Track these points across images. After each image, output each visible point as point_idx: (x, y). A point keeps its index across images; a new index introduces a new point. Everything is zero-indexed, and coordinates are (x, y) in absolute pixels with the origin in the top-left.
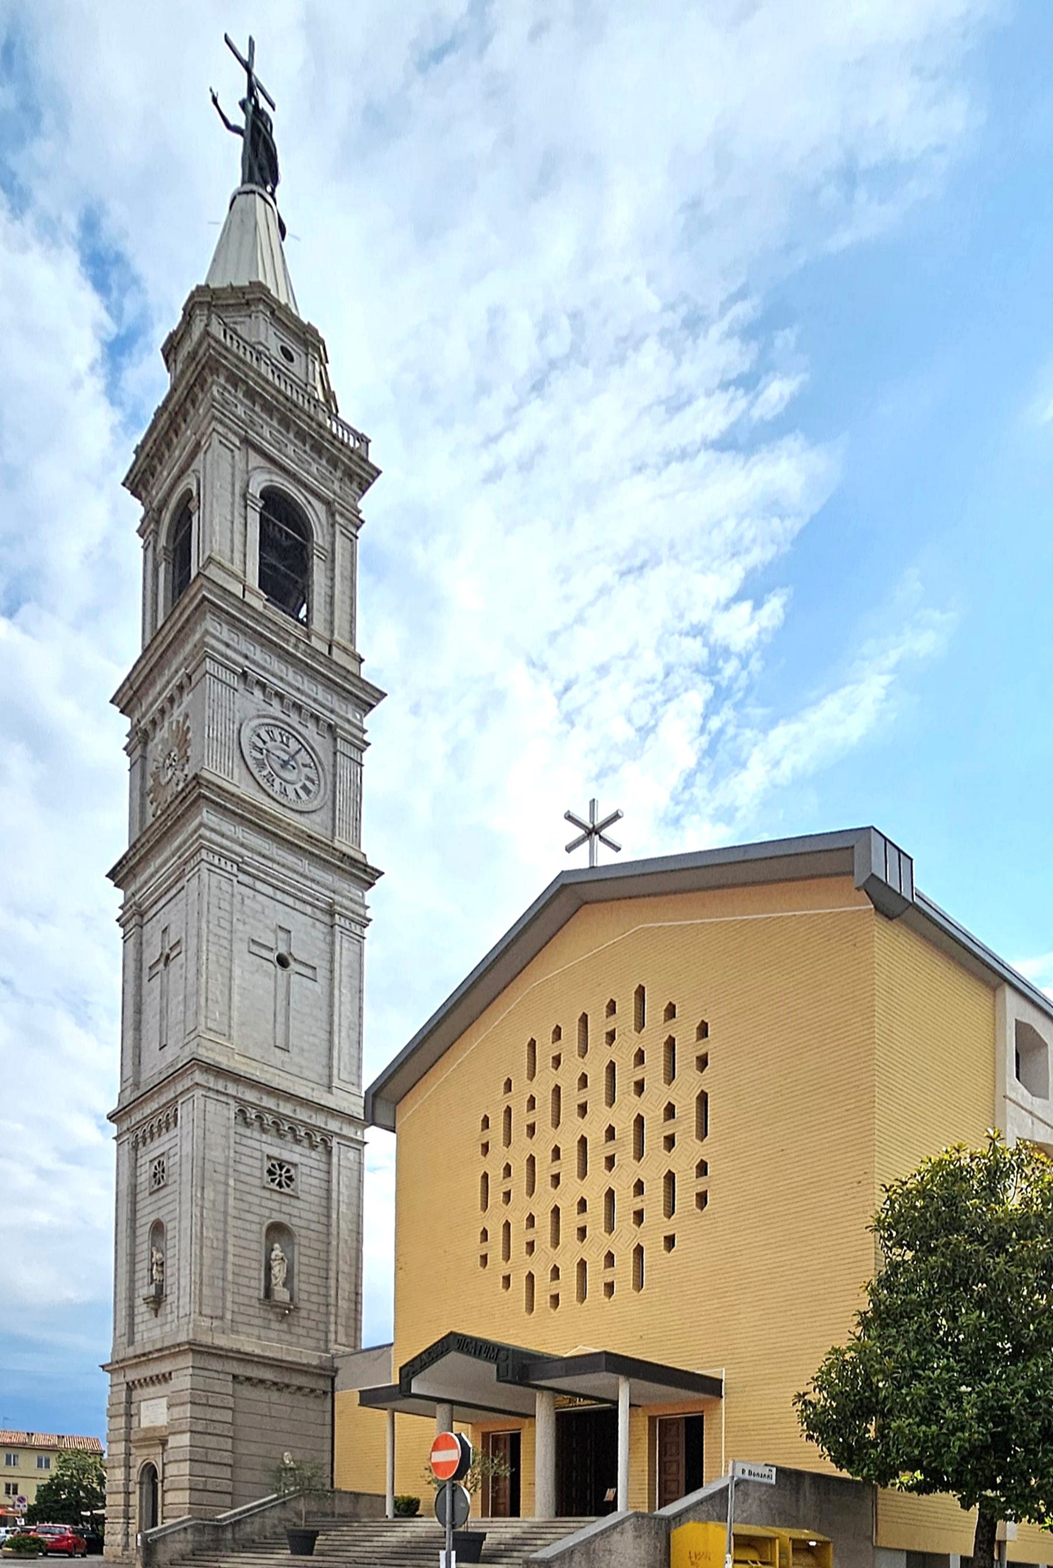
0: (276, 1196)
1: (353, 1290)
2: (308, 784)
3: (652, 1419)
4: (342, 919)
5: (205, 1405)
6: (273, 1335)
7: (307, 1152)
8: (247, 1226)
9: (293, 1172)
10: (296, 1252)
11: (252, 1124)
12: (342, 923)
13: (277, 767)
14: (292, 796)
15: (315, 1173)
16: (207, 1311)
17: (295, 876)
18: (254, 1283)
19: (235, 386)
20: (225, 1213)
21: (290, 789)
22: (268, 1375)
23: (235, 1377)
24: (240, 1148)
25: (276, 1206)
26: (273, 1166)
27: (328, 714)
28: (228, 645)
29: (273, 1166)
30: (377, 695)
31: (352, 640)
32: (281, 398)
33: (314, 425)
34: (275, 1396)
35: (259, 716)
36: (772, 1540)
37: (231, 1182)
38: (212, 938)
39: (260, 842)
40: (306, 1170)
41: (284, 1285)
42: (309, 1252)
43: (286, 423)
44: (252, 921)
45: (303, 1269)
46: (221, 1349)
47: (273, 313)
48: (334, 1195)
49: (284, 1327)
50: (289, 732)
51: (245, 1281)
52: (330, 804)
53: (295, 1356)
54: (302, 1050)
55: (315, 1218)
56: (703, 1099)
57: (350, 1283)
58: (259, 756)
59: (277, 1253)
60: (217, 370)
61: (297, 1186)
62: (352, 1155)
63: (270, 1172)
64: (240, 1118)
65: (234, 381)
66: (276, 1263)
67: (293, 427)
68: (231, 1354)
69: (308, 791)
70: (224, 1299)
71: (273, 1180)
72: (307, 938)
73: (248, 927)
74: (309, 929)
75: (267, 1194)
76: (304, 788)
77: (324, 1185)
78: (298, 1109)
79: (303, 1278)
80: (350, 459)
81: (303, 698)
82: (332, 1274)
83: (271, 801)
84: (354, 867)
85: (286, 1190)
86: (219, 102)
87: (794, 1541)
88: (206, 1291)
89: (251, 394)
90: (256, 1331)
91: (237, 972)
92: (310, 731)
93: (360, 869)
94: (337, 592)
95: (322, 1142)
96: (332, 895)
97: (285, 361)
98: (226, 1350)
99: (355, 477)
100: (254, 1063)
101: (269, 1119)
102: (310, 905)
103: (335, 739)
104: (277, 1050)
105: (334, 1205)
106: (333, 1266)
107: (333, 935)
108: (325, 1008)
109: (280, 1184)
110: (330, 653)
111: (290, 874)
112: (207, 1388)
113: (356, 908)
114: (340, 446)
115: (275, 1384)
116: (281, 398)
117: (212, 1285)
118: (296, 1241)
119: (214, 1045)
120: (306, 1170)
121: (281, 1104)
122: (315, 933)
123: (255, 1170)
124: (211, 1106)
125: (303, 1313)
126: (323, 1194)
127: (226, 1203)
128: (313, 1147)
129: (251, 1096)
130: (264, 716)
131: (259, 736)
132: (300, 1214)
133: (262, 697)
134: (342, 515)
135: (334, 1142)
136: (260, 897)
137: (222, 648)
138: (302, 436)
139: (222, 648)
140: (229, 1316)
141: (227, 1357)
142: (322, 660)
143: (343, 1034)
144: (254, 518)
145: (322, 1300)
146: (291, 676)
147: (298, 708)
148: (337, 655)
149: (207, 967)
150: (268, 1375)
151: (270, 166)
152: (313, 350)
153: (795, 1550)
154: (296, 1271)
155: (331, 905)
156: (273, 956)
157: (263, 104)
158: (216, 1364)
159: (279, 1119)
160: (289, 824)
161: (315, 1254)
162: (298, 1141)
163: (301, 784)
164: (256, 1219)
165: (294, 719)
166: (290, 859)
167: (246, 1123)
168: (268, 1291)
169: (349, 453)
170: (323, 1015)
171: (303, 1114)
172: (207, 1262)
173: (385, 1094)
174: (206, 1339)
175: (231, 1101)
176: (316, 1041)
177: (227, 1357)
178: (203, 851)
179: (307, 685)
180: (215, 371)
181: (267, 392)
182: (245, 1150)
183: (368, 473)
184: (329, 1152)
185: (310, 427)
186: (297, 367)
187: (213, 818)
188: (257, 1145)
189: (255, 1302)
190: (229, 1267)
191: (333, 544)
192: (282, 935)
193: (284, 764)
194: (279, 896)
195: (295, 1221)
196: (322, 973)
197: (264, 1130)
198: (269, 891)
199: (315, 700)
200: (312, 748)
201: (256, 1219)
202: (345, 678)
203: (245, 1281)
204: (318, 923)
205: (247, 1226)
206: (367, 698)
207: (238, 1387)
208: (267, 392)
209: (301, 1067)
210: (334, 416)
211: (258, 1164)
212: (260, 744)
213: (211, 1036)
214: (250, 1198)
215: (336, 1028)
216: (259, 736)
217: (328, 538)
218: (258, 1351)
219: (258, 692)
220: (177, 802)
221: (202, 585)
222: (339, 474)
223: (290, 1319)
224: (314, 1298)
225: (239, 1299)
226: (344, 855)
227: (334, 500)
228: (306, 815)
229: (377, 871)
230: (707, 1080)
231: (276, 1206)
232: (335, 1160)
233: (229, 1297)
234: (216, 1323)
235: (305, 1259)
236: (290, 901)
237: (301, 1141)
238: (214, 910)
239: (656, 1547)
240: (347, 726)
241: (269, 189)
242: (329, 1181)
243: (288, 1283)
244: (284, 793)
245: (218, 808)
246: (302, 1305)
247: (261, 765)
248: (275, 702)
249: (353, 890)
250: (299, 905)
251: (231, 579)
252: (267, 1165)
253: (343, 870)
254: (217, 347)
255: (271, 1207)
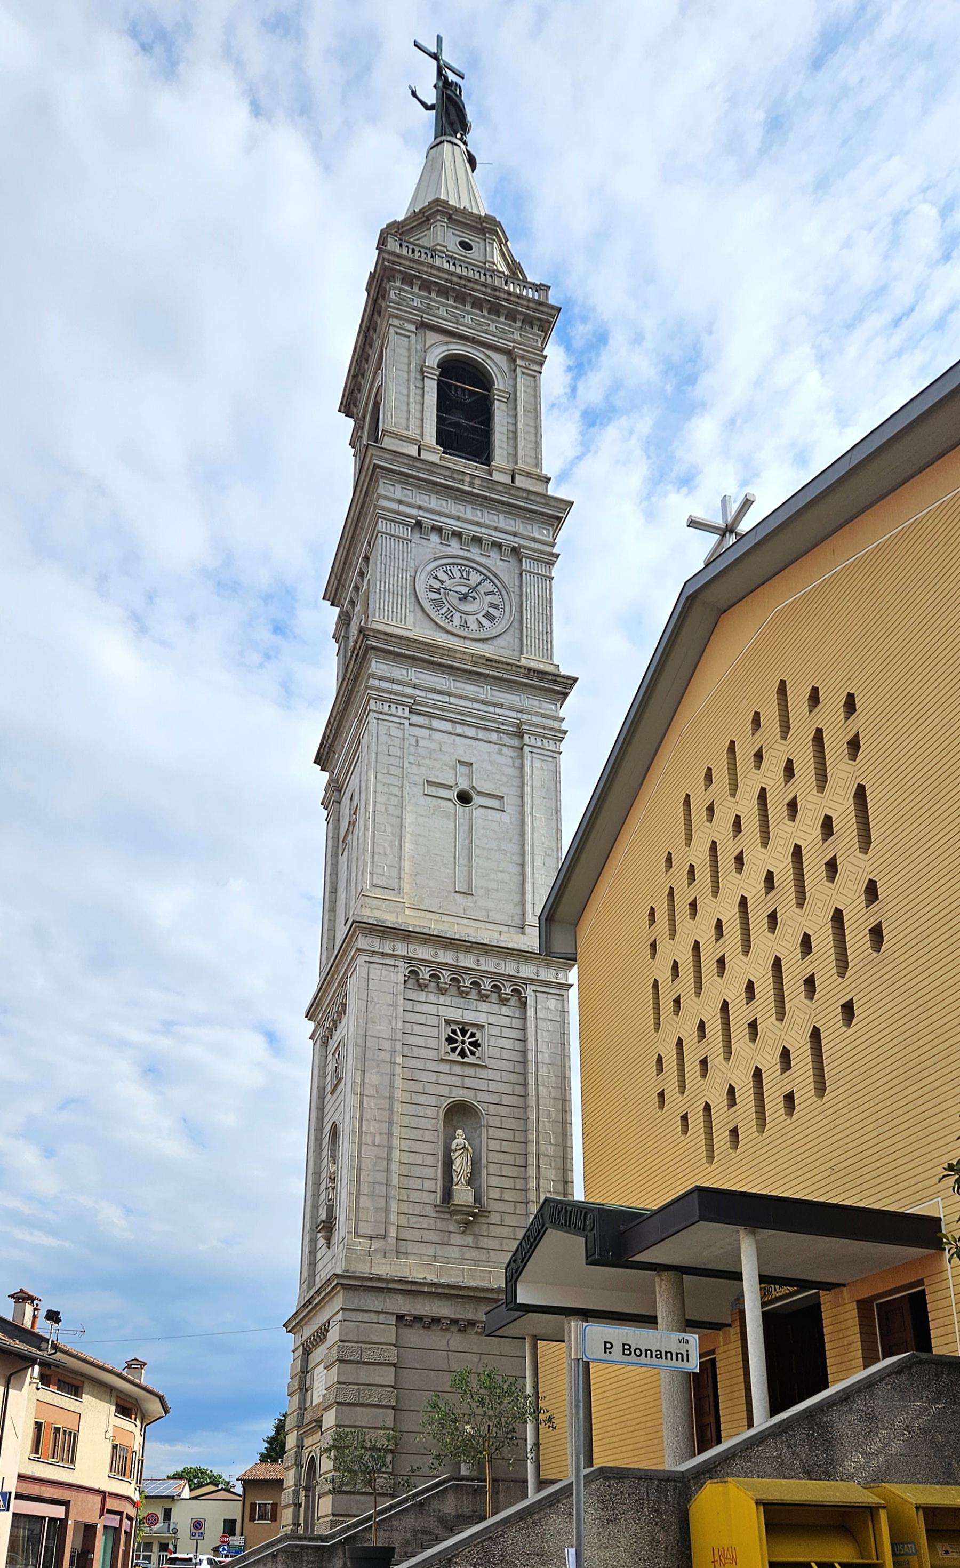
0: (457, 1069)
1: (560, 1177)
2: (492, 611)
3: (864, 1306)
4: (532, 738)
5: (357, 1362)
6: (454, 1252)
7: (495, 1008)
8: (421, 1111)
9: (478, 1036)
10: (484, 1136)
11: (426, 986)
12: (533, 742)
13: (455, 602)
14: (474, 626)
15: (507, 1033)
16: (366, 1229)
17: (476, 705)
18: (428, 1185)
19: (411, 285)
20: (391, 1098)
21: (471, 620)
22: (444, 1310)
23: (400, 1318)
24: (411, 1017)
25: (457, 1081)
26: (454, 1032)
27: (511, 538)
28: (420, 508)
29: (454, 1032)
30: (563, 506)
31: (538, 463)
32: (455, 279)
33: (489, 291)
34: (456, 1340)
35: (435, 559)
36: (871, 1511)
37: (399, 1060)
38: (380, 788)
39: (437, 679)
40: (495, 1031)
41: (469, 1182)
42: (501, 1134)
43: (461, 298)
44: (427, 761)
45: (495, 1157)
46: (380, 1279)
47: (450, 218)
48: (531, 1056)
49: (469, 1240)
50: (467, 565)
51: (417, 1184)
52: (516, 625)
53: (482, 1279)
54: (488, 890)
55: (507, 1089)
56: (860, 794)
57: (557, 1169)
58: (437, 596)
59: (460, 1141)
60: (394, 277)
61: (483, 1052)
62: (552, 1003)
63: (450, 1040)
64: (411, 982)
65: (408, 280)
66: (457, 1154)
67: (469, 299)
68: (391, 1286)
69: (496, 607)
70: (387, 1211)
71: (453, 1050)
72: (490, 763)
73: (422, 769)
74: (495, 757)
75: (444, 1067)
76: (492, 605)
77: (518, 1046)
78: (482, 960)
79: (493, 1169)
80: (528, 308)
81: (483, 530)
82: (532, 1160)
83: (450, 637)
84: (542, 680)
85: (470, 1059)
86: (417, 93)
87: (931, 1513)
88: (365, 1202)
89: (426, 286)
90: (430, 1250)
91: (409, 818)
92: (494, 561)
93: (549, 681)
94: (519, 426)
95: (514, 995)
96: (519, 715)
97: (463, 252)
98: (388, 1281)
99: (535, 322)
100: (429, 915)
101: (446, 976)
102: (497, 731)
103: (521, 561)
104: (457, 895)
105: (532, 1068)
106: (532, 1148)
107: (522, 757)
108: (516, 838)
109: (463, 1054)
110: (513, 482)
111: (469, 704)
112: (362, 1338)
113: (549, 723)
114: (516, 300)
115: (454, 1322)
116: (455, 279)
117: (372, 1195)
118: (484, 1122)
119: (380, 902)
120: (495, 1031)
121: (461, 956)
122: (502, 760)
123: (432, 1039)
124: (376, 971)
125: (494, 1218)
126: (517, 1057)
127: (391, 1086)
128: (503, 1001)
129: (423, 952)
130: (441, 558)
131: (436, 578)
132: (486, 1087)
133: (438, 541)
134: (522, 358)
135: (529, 992)
136: (436, 735)
137: (394, 506)
138: (478, 304)
139: (394, 506)
140: (393, 1233)
141: (390, 1290)
142: (500, 488)
143: (539, 862)
144: (432, 387)
145: (517, 1196)
146: (469, 512)
147: (477, 540)
148: (520, 481)
149: (374, 820)
150: (444, 1310)
151: (459, 119)
152: (489, 233)
153: (933, 1534)
154: (484, 1161)
155: (518, 726)
156: (452, 795)
157: (452, 77)
158: (374, 1302)
159: (458, 972)
160: (465, 653)
161: (509, 1135)
162: (484, 998)
163: (484, 612)
164: (433, 1100)
165: (475, 553)
166: (470, 689)
167: (420, 985)
168: (447, 1194)
169: (525, 303)
170: (513, 848)
171: (488, 964)
172: (366, 1164)
173: (560, 913)
174: (363, 1269)
175: (400, 964)
176: (506, 877)
177: (390, 1290)
178: (372, 702)
179: (488, 518)
180: (391, 278)
181: (440, 278)
182: (420, 1018)
183: (548, 314)
184: (524, 1004)
185: (484, 293)
186: (476, 254)
187: (384, 667)
188: (432, 1009)
189: (429, 1210)
190: (395, 1167)
191: (515, 386)
192: (464, 770)
193: (464, 598)
194: (459, 729)
195: (482, 1096)
196: (510, 803)
197: (442, 991)
198: (448, 726)
199: (496, 529)
200: (495, 575)
201: (433, 1100)
202: (527, 499)
203: (417, 1184)
204: (505, 749)
205: (421, 1111)
206: (554, 514)
207: (406, 1331)
208: (440, 278)
209: (487, 911)
210: (525, 283)
211: (434, 1032)
212: (437, 585)
213: (378, 893)
214: (424, 1076)
215: (528, 858)
216: (436, 578)
217: (511, 382)
218: (431, 1278)
219: (435, 538)
220: (352, 662)
221: (372, 455)
222: (519, 324)
223: (476, 1229)
224: (508, 1195)
225: (405, 1208)
226: (530, 670)
227: (514, 347)
228: (490, 642)
229: (568, 678)
230: (864, 770)
231: (457, 1081)
232: (530, 1012)
233: (394, 1207)
234: (376, 1244)
235: (493, 1144)
236: (471, 732)
237: (487, 996)
238: (383, 758)
239: (654, 1542)
240: (533, 545)
241: (459, 136)
242: (524, 1041)
243: (472, 1180)
244: (465, 625)
245: (388, 656)
246: (493, 1206)
247: (438, 604)
248: (454, 543)
249: (545, 705)
250: (481, 734)
251: (405, 444)
252: (446, 1032)
253: (531, 686)
254: (391, 258)
255: (452, 1084)
